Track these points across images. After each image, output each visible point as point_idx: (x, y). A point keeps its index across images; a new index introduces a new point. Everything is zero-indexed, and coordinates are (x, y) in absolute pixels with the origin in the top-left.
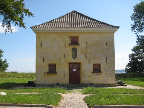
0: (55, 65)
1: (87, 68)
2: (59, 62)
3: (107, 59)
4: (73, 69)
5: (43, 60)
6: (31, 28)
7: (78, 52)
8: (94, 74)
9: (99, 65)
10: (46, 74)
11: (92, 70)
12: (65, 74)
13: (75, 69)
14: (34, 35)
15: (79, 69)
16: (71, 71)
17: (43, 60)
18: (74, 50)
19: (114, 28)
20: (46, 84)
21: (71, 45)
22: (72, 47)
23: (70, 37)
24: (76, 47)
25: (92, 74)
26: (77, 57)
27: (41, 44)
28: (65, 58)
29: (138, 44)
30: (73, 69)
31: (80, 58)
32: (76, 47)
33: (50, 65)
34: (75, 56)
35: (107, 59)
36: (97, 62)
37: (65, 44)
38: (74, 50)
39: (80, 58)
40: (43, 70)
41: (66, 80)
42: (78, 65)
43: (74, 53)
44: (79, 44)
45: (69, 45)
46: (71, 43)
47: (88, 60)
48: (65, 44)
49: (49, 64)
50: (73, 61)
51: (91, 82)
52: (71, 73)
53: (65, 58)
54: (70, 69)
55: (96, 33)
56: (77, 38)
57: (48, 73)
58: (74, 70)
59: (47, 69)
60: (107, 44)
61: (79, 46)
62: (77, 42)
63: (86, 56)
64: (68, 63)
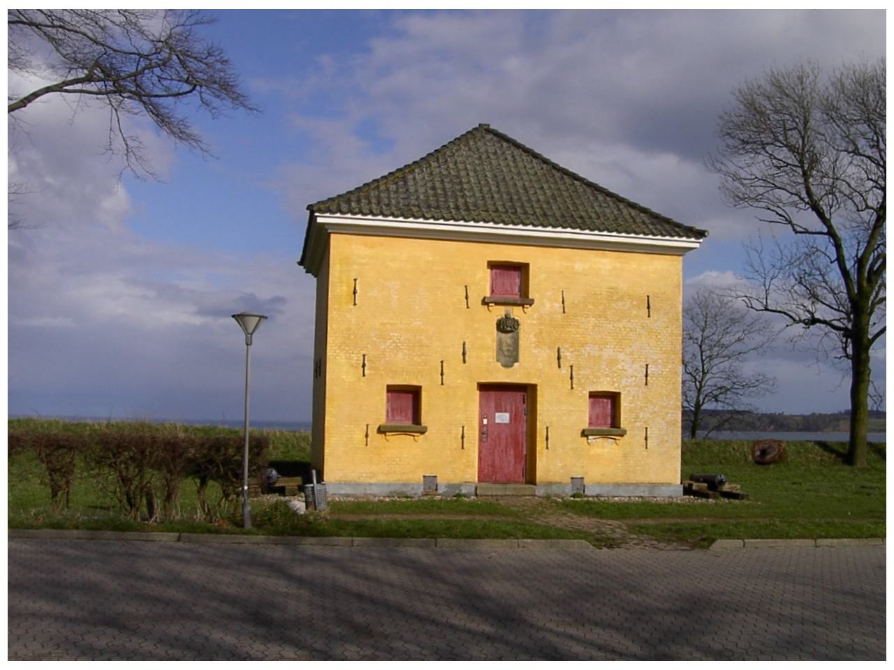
13: (507, 415)
16: (485, 421)
18: (506, 326)
22: (499, 312)
24: (516, 312)
47: (565, 371)
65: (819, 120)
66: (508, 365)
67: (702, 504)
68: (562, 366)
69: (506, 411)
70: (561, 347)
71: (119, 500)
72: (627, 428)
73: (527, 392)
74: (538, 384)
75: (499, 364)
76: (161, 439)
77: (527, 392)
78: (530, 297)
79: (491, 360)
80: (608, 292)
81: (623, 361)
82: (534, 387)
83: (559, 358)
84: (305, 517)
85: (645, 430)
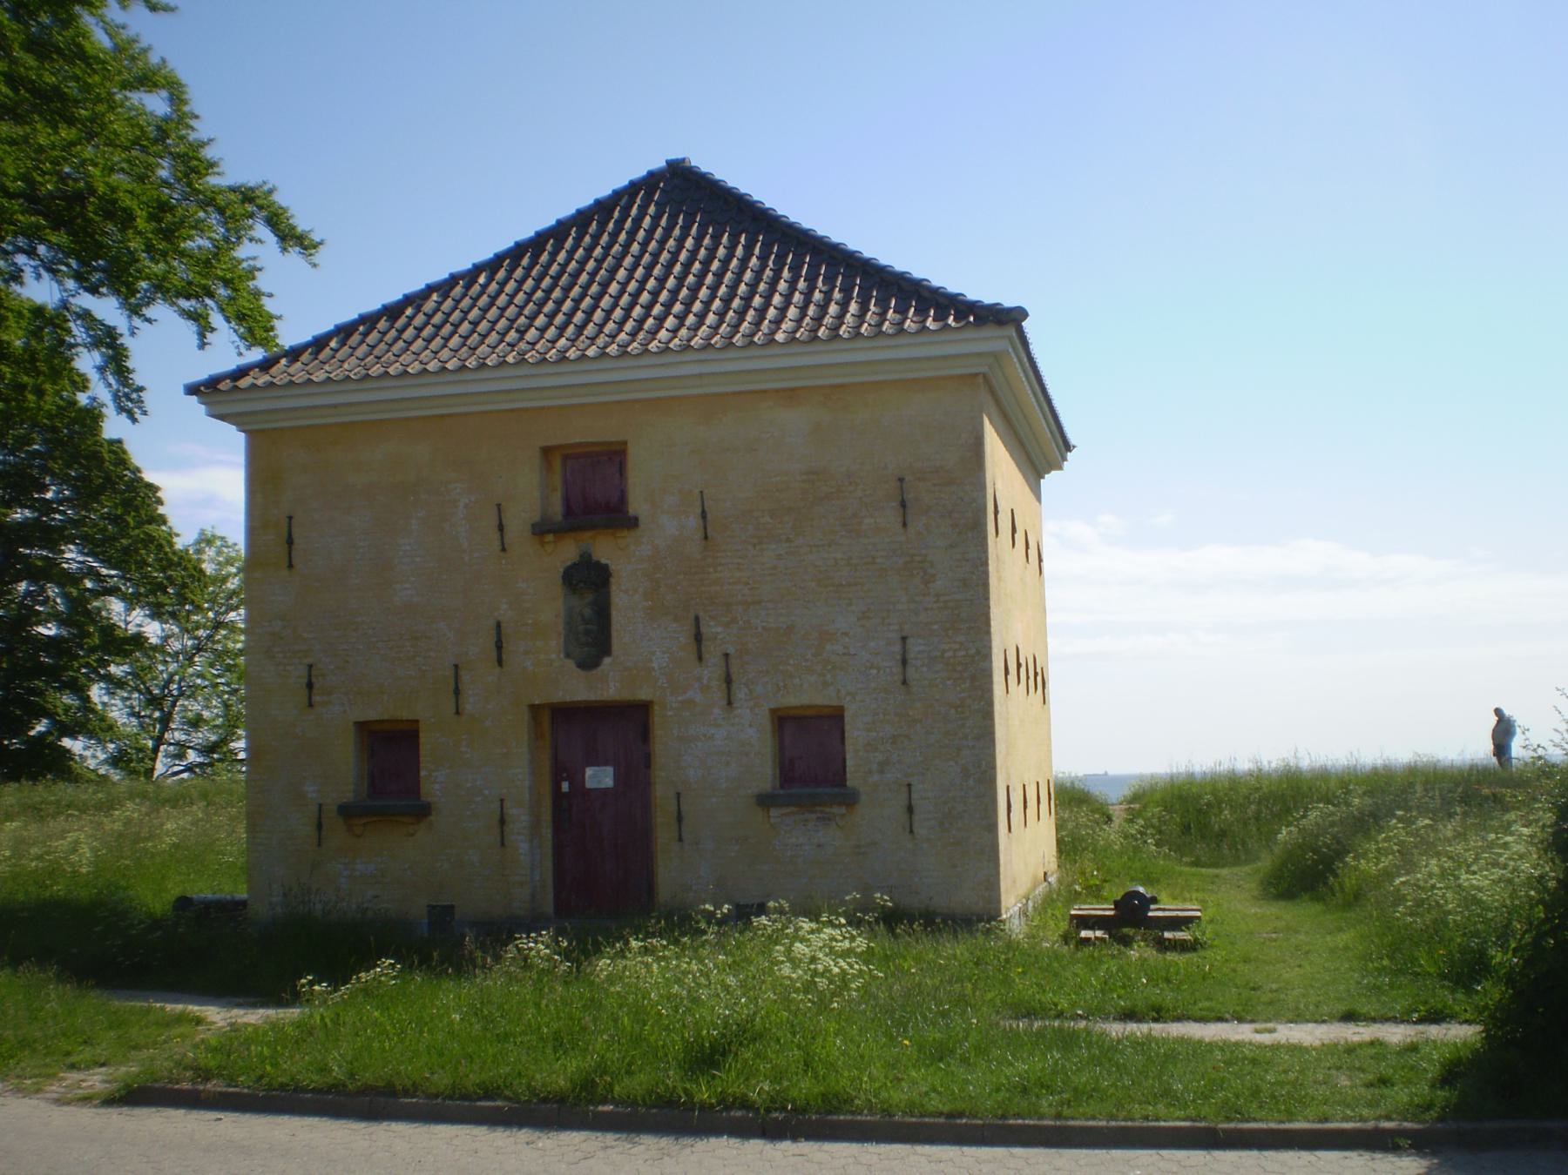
0: (833, 719)
1: (712, 752)
2: (916, 647)
3: (904, 662)
4: (589, 771)
5: (310, 685)
6: (192, 390)
7: (625, 602)
8: (774, 812)
9: (833, 719)
11: (764, 775)
12: (502, 821)
13: (610, 770)
14: (233, 440)
16: (565, 786)
17: (310, 685)
19: (971, 333)
21: (550, 538)
22: (567, 552)
23: (547, 451)
24: (604, 549)
27: (290, 541)
28: (500, 662)
30: (589, 771)
31: (645, 653)
32: (604, 549)
33: (784, 721)
35: (904, 662)
36: (806, 694)
37: (501, 528)
38: (589, 580)
39: (645, 653)
40: (310, 790)
41: (529, 860)
42: (626, 725)
43: (587, 612)
44: (633, 523)
45: (542, 530)
46: (569, 511)
47: (711, 672)
48: (501, 528)
49: (362, 726)
50: (578, 688)
52: (570, 813)
53: (500, 662)
54: (564, 769)
55: (790, 396)
56: (614, 457)
59: (342, 770)
60: (903, 504)
62: (623, 499)
63: (698, 638)
65: (80, 349)
66: (589, 663)
68: (706, 656)
69: (606, 764)
70: (701, 614)
73: (632, 719)
75: (570, 664)
77: (632, 719)
79: (553, 656)
81: (846, 634)
84: (1498, 1021)
85: (905, 789)
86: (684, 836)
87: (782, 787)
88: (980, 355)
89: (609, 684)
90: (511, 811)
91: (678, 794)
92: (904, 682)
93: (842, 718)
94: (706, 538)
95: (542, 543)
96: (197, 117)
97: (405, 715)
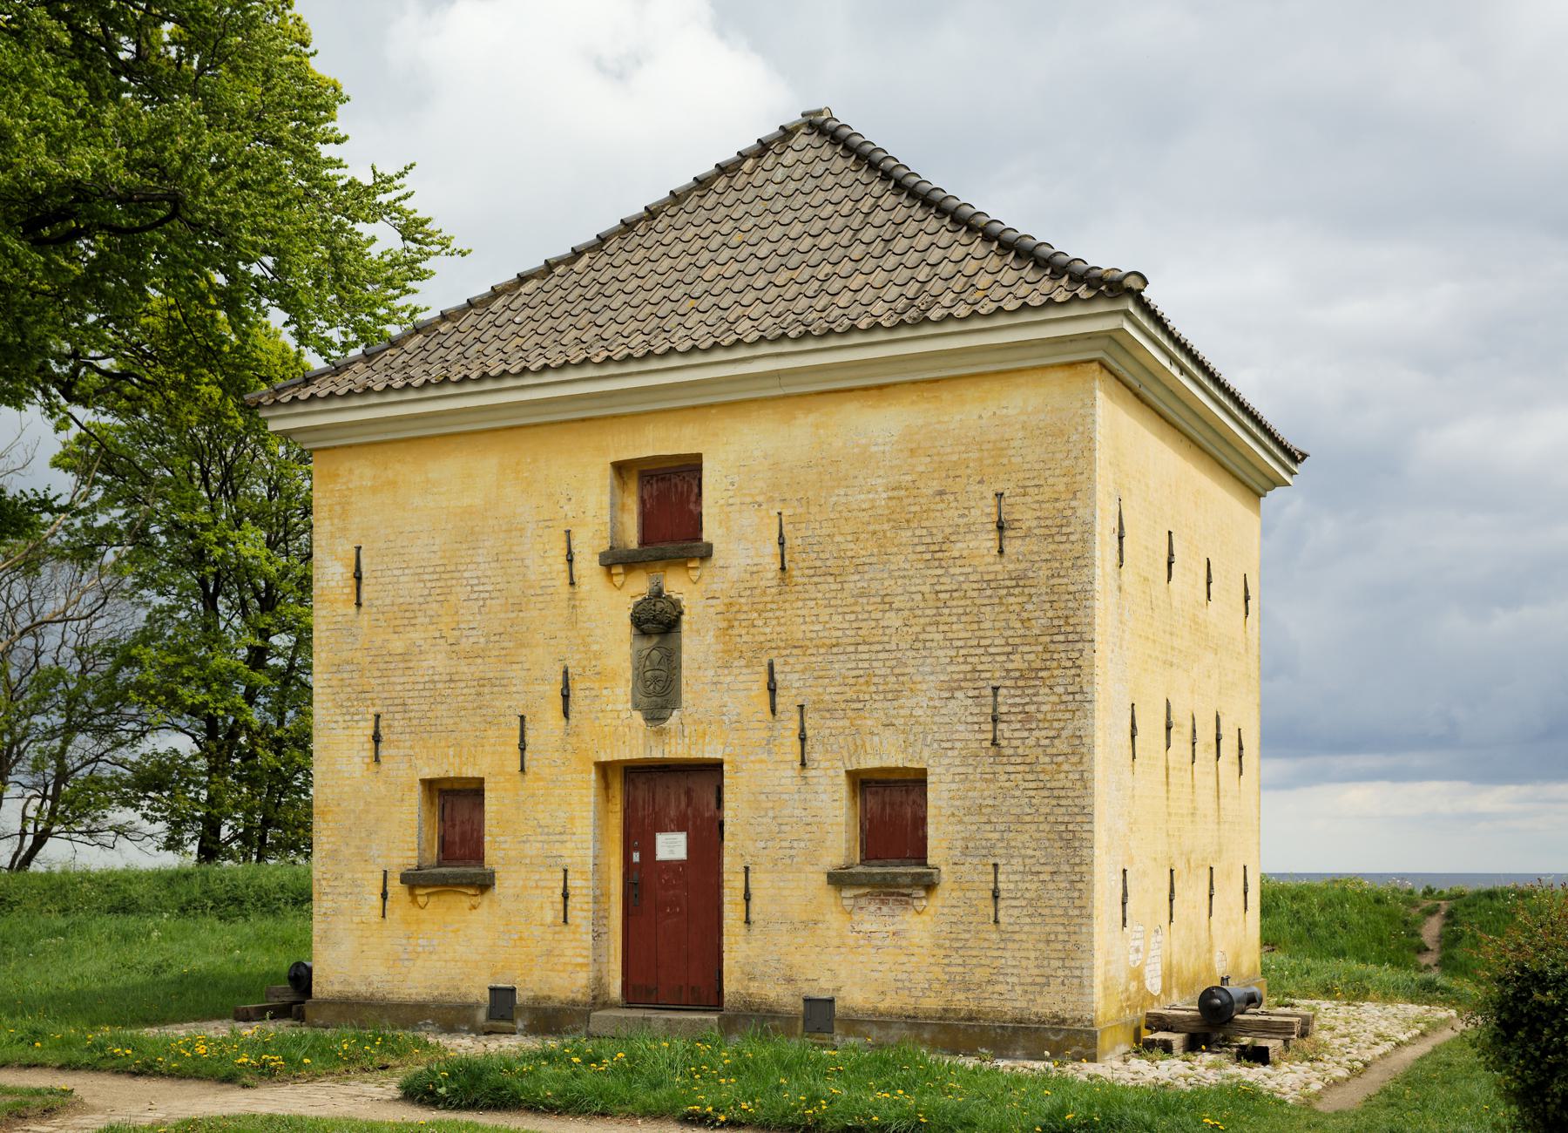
0: (915, 782)
7: (697, 644)
10: (395, 885)
13: (681, 838)
15: (708, 838)
16: (636, 857)
18: (658, 624)
20: (395, 998)
22: (639, 586)
24: (676, 584)
25: (828, 896)
26: (687, 696)
29: (333, 584)
33: (864, 783)
34: (659, 692)
36: (886, 754)
38: (658, 624)
45: (616, 561)
49: (429, 785)
51: (822, 987)
52: (643, 885)
54: (637, 836)
57: (414, 880)
58: (671, 846)
61: (696, 571)
64: (604, 768)
67: (1045, 1078)
71: (113, 910)
72: (946, 877)
74: (726, 759)
76: (1514, 1109)
78: (706, 537)
80: (890, 498)
82: (714, 768)
83: (772, 690)
86: (753, 917)
87: (862, 862)
88: (1089, 337)
89: (677, 747)
90: (575, 882)
91: (747, 869)
92: (994, 743)
93: (925, 782)
94: (783, 568)
95: (610, 575)
96: (427, 222)
97: (469, 772)
